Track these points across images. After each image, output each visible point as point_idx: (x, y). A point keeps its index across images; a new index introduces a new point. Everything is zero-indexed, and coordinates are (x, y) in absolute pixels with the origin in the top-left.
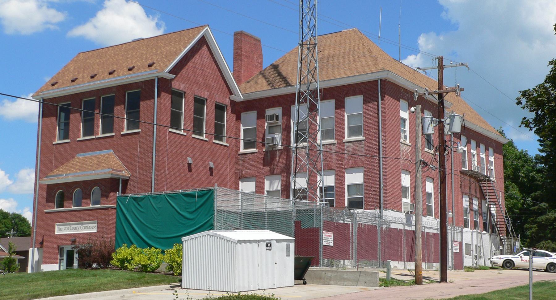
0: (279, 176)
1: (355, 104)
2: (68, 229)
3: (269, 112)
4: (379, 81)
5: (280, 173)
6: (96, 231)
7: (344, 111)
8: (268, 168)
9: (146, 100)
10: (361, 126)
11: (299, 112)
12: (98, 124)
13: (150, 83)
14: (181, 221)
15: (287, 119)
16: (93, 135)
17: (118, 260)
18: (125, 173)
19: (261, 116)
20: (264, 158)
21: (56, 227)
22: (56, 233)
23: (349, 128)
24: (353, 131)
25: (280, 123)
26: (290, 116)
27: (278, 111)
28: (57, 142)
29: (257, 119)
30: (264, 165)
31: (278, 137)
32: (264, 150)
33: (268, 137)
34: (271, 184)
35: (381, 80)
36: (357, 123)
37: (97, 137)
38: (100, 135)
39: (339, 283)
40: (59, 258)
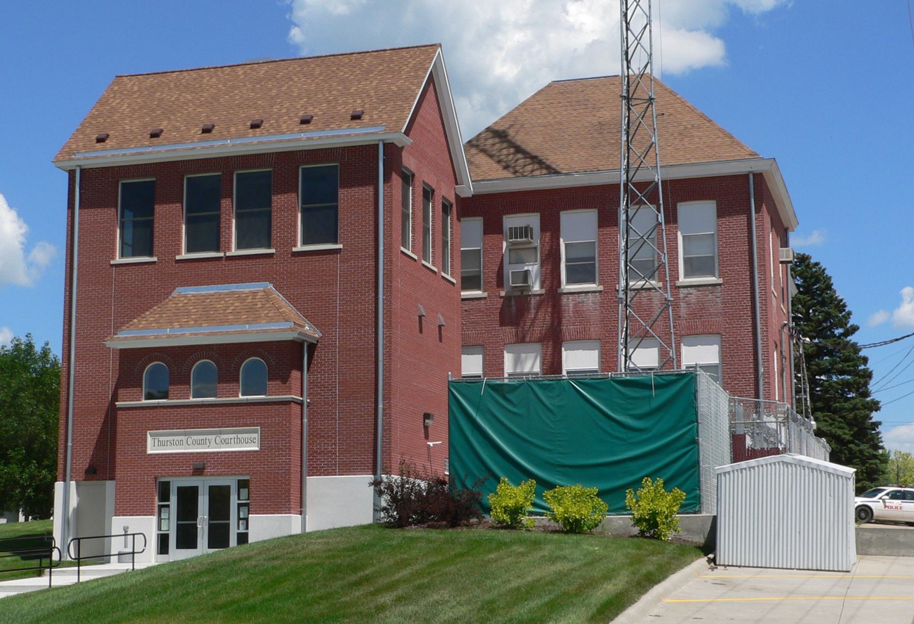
0: (538, 346)
1: (699, 216)
2: (180, 443)
3: (511, 221)
4: (751, 177)
5: (540, 341)
6: (257, 449)
7: (676, 228)
8: (509, 330)
9: (354, 186)
10: (712, 258)
11: (579, 227)
12: (230, 228)
13: (367, 152)
14: (616, 434)
15: (552, 236)
16: (218, 249)
17: (506, 510)
18: (309, 330)
19: (493, 227)
20: (502, 309)
21: (149, 438)
22: (149, 452)
23: (686, 261)
24: (693, 267)
25: (537, 242)
26: (559, 230)
27: (532, 220)
28: (118, 260)
29: (485, 233)
30: (502, 323)
31: (534, 269)
32: (503, 294)
33: (509, 270)
34: (517, 362)
35: (754, 175)
36: (703, 251)
37: (228, 254)
38: (234, 252)
39: (887, 552)
40: (157, 503)
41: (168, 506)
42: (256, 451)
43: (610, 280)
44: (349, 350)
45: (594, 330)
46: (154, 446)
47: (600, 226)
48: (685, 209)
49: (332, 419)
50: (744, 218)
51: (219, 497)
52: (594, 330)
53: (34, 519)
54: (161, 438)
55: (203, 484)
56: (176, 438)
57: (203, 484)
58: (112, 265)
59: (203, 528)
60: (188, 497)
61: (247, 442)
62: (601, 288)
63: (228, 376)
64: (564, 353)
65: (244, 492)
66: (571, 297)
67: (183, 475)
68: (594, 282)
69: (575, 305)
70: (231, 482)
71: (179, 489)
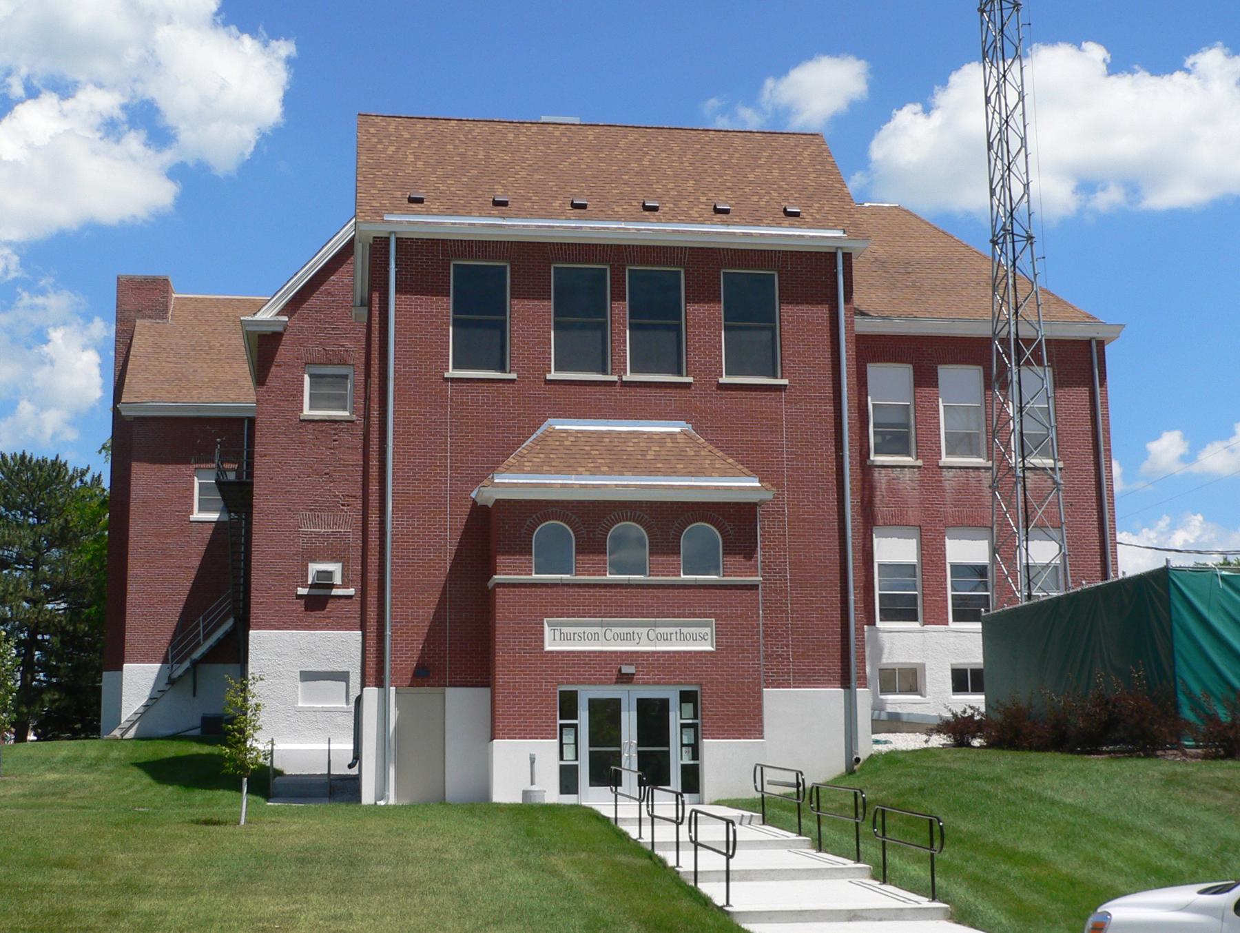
2: (595, 636)
6: (710, 648)
21: (547, 629)
22: (548, 648)
24: (960, 443)
41: (575, 726)
42: (711, 652)
43: (929, 451)
44: (804, 520)
45: (913, 514)
46: (559, 638)
47: (915, 386)
48: (947, 373)
49: (782, 612)
50: (1085, 391)
51: (653, 719)
52: (913, 514)
53: (41, 738)
54: (564, 630)
55: (629, 698)
56: (588, 630)
57: (629, 698)
58: (447, 379)
59: (630, 757)
60: (605, 714)
61: (697, 639)
62: (920, 463)
63: (591, 545)
64: (875, 541)
65: (688, 708)
66: (883, 472)
67: (602, 683)
68: (908, 454)
69: (889, 481)
70: (672, 694)
71: (591, 701)
